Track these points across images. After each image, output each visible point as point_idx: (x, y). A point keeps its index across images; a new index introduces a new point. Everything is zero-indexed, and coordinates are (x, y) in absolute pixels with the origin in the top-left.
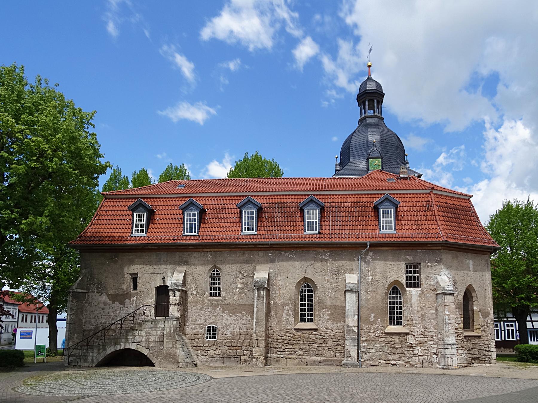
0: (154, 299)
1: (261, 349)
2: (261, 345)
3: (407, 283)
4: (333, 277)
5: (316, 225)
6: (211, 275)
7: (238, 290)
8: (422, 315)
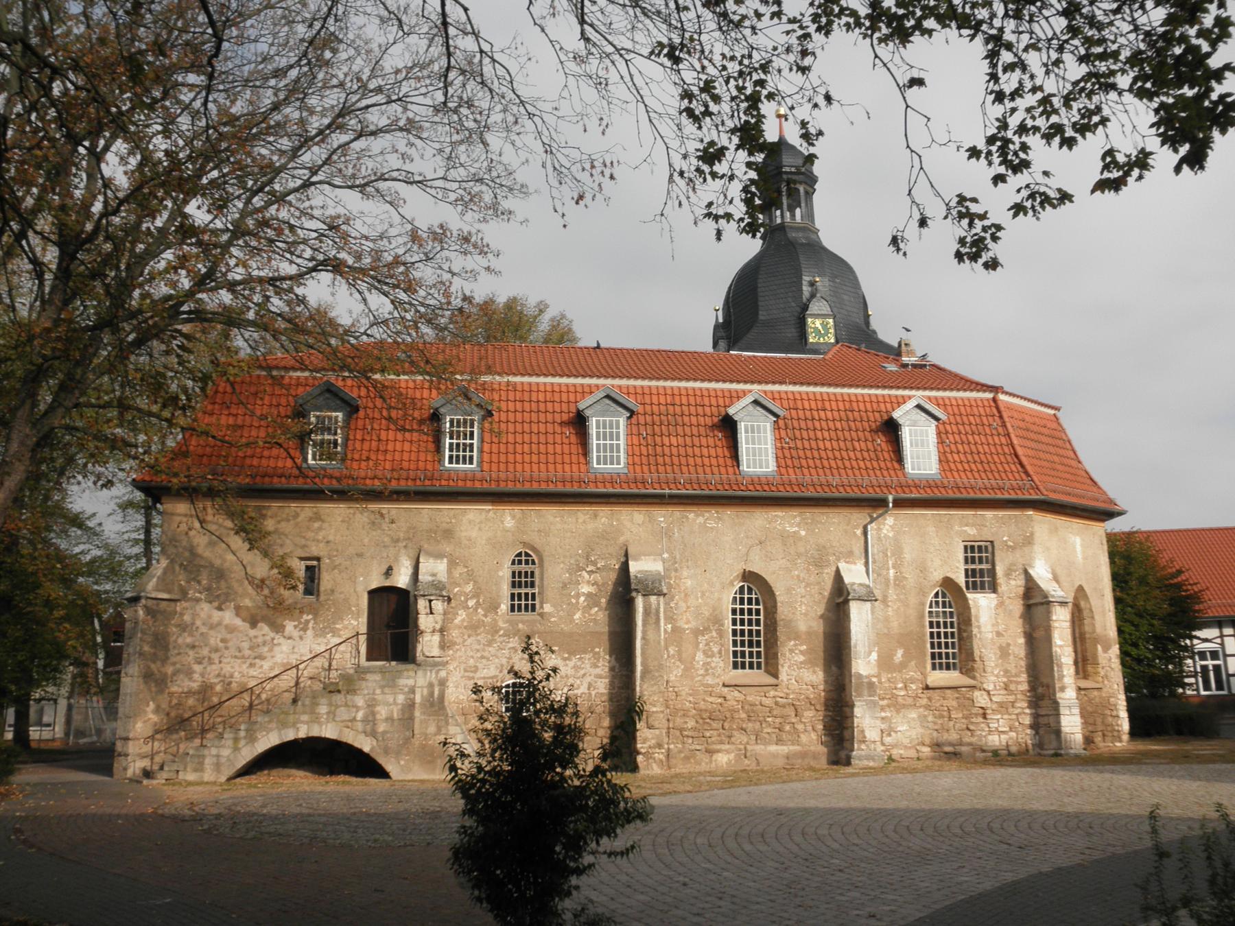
0: (364, 619)
1: (657, 732)
2: (656, 724)
3: (967, 582)
4: (808, 570)
5: (618, 451)
6: (513, 563)
7: (582, 599)
8: (1001, 648)
